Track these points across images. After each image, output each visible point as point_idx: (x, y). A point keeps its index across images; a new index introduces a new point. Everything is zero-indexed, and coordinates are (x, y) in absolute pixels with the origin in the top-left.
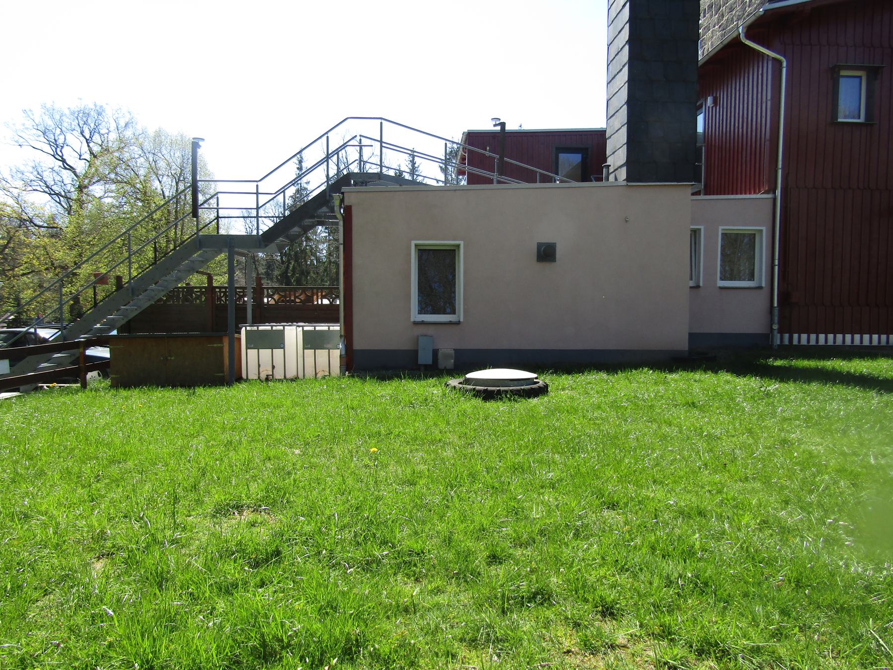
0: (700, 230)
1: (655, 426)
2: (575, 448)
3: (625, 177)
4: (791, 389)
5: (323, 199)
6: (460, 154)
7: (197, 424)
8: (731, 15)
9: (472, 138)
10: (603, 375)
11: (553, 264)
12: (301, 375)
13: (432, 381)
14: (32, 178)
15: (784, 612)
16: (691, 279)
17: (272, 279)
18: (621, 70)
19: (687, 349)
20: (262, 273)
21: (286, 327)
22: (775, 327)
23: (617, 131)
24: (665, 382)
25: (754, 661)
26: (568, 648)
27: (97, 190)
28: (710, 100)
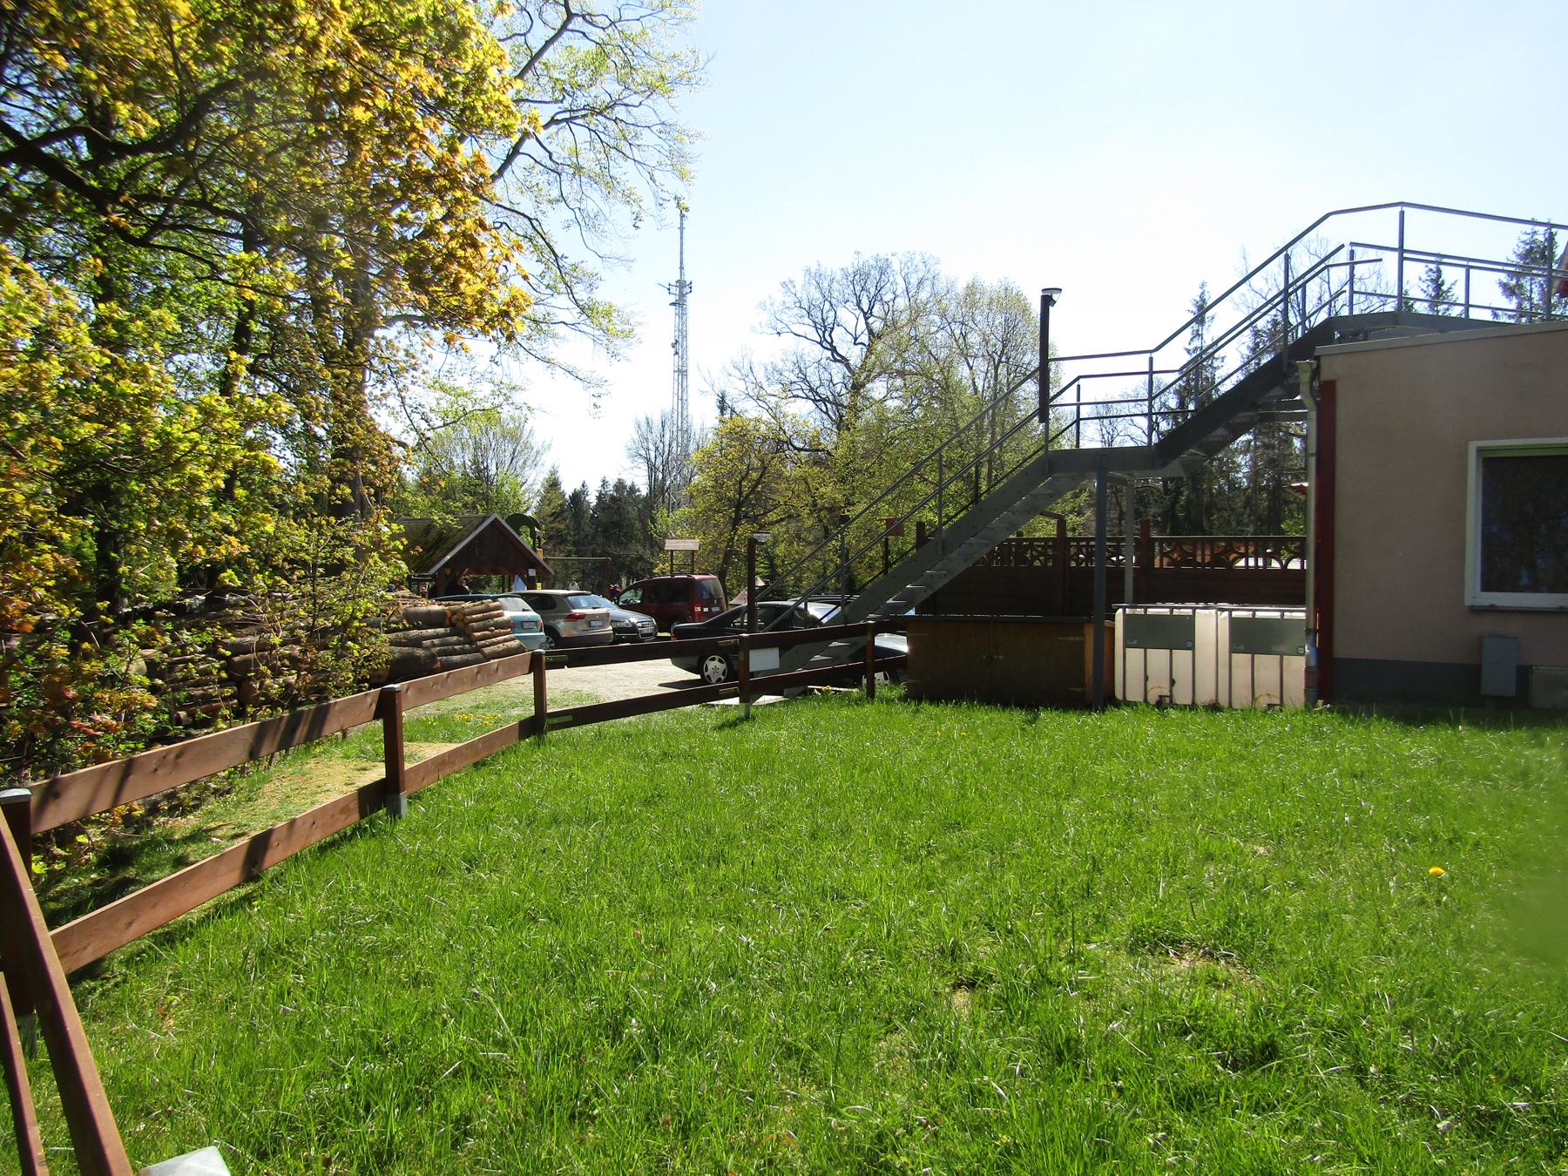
7: (1066, 777)
10: (1019, 716)
12: (1223, 701)
14: (795, 379)
27: (877, 389)
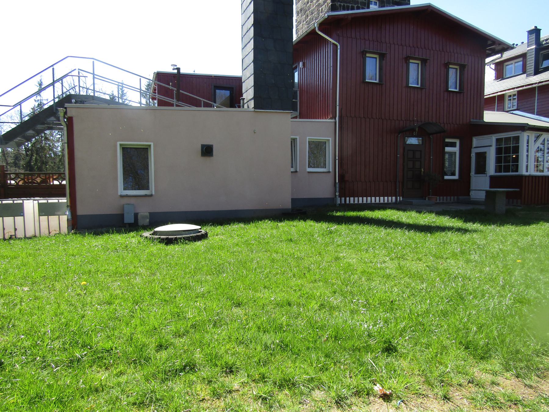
0: (297, 138)
1: (268, 254)
2: (219, 270)
3: (253, 106)
4: (343, 228)
5: (52, 111)
6: (152, 86)
8: (312, 16)
9: (160, 76)
10: (242, 225)
11: (211, 158)
13: (132, 234)
15: (327, 356)
16: (292, 167)
17: (19, 167)
18: (249, 42)
19: (290, 207)
20: (11, 163)
21: (24, 201)
22: (337, 194)
23: (248, 78)
24: (277, 227)
25: (310, 386)
26: (203, 397)
28: (301, 64)
